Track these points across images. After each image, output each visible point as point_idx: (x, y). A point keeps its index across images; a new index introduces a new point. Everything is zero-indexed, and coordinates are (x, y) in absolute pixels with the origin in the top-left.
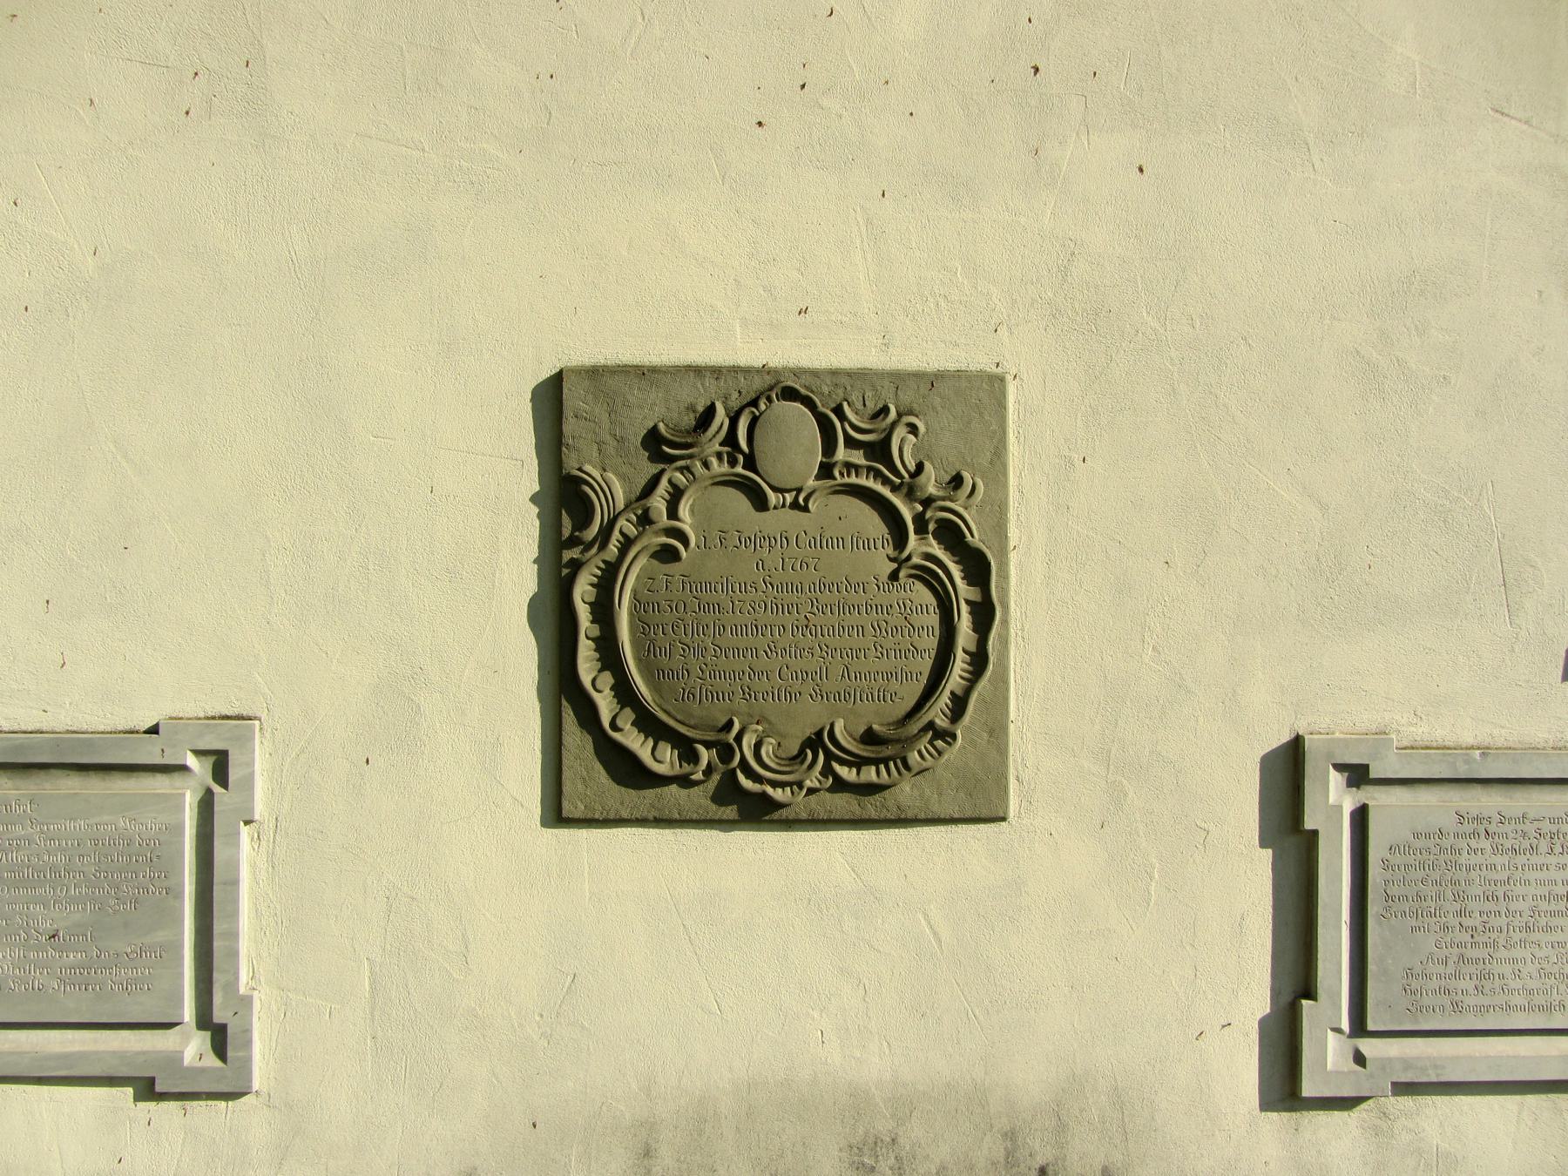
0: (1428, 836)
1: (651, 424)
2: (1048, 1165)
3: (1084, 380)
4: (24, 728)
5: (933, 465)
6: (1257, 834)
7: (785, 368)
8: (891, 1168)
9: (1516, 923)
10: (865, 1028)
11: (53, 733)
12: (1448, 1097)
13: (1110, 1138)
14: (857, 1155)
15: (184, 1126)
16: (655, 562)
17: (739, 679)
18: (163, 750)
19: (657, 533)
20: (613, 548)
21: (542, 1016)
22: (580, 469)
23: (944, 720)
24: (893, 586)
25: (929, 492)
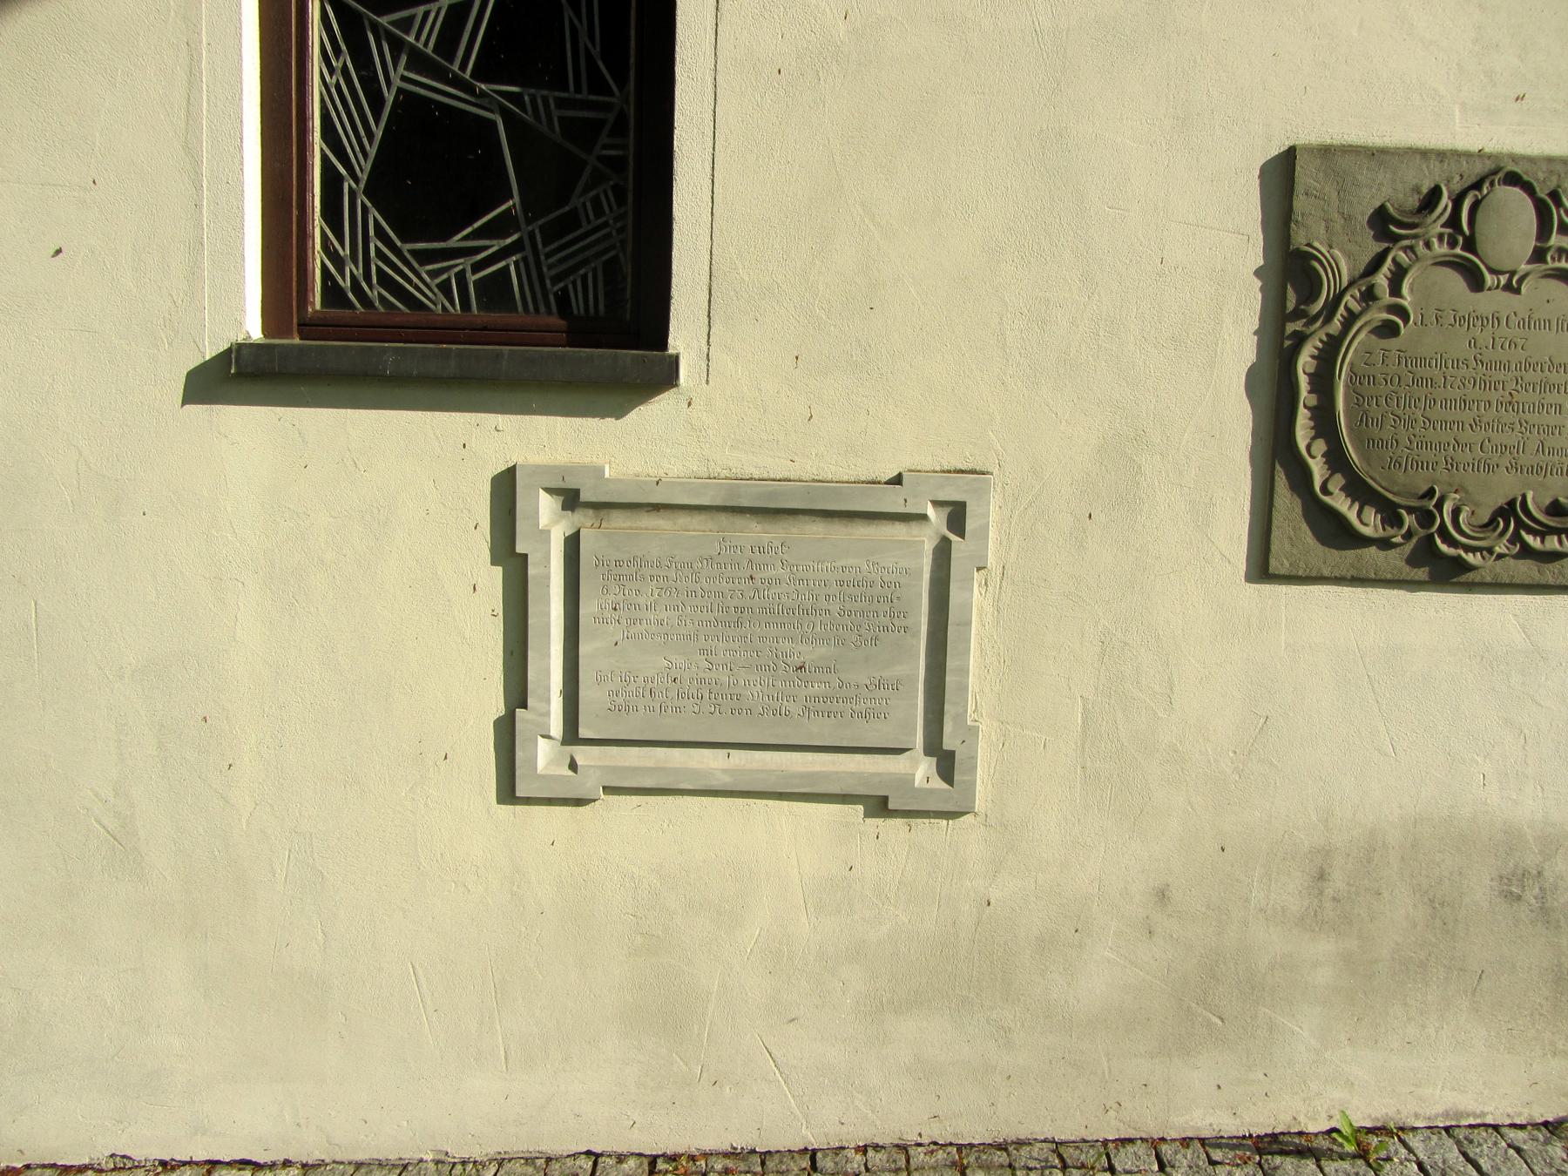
1: (1378, 204)
4: (772, 476)
7: (1448, 150)
8: (1535, 898)
11: (800, 481)
14: (1506, 884)
15: (909, 840)
16: (1373, 337)
17: (1444, 450)
18: (906, 501)
19: (1380, 310)
20: (1336, 325)
21: (1235, 753)
22: (1309, 245)
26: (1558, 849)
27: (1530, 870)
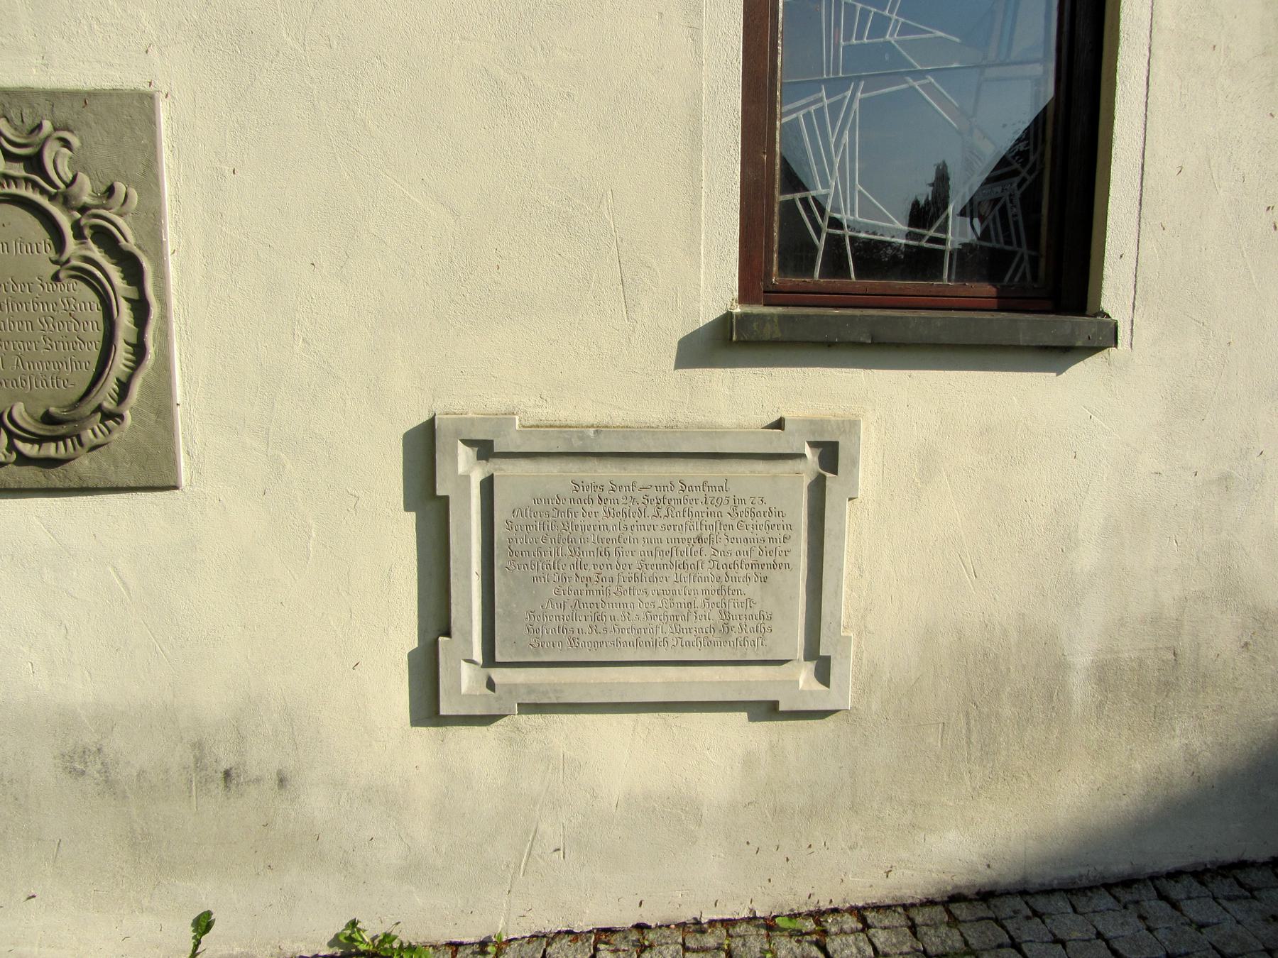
0: (547, 501)
2: (231, 769)
3: (230, 98)
5: (89, 176)
6: (402, 499)
8: (99, 772)
9: (626, 574)
10: (68, 660)
12: (573, 715)
13: (283, 748)
23: (111, 403)
24: (57, 286)
25: (83, 201)
26: (113, 728)
27: (89, 747)
